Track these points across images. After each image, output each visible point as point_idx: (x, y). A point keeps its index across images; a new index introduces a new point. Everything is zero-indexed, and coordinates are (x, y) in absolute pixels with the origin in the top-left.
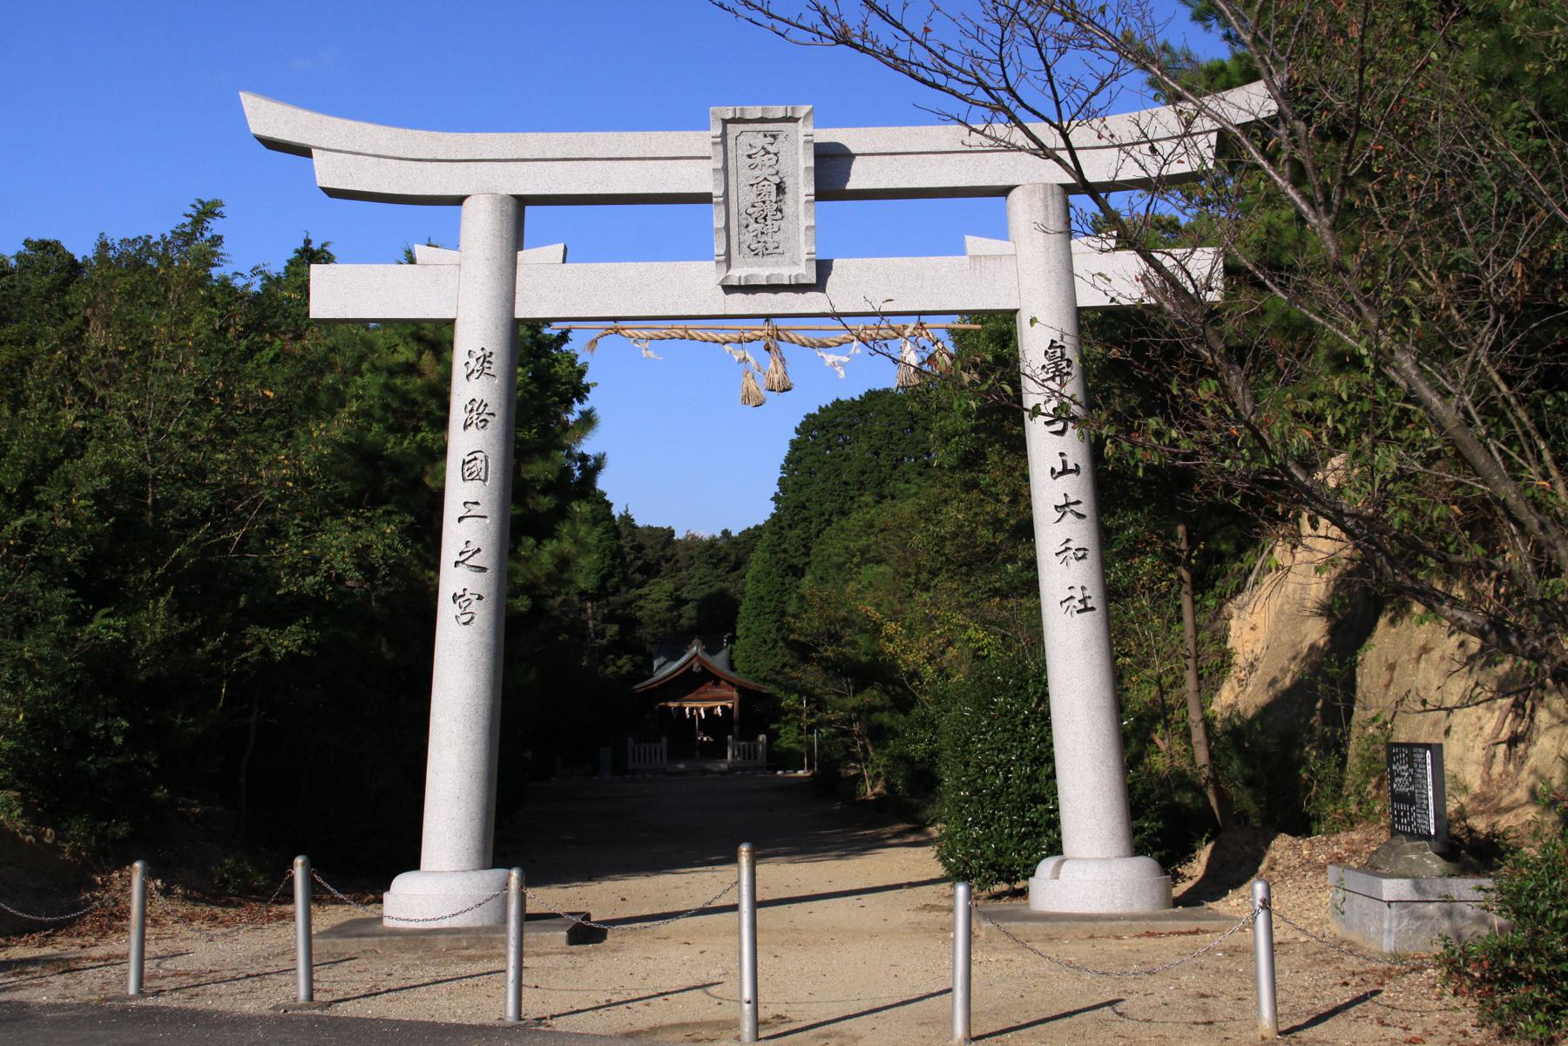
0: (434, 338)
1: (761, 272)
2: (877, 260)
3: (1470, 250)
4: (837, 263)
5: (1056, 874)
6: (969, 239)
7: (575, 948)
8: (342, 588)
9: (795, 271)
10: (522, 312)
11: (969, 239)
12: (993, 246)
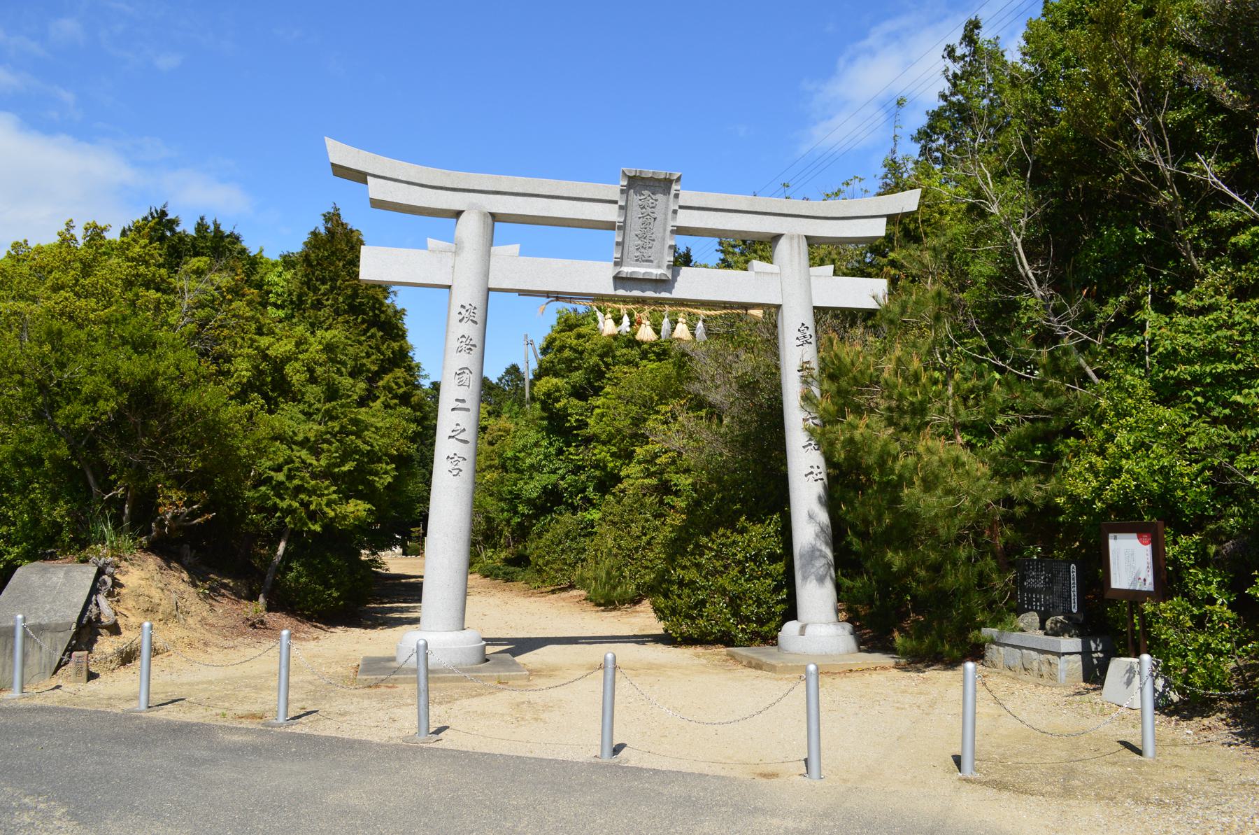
0: (773, 311)
1: (641, 270)
3: (170, 354)
9: (659, 271)
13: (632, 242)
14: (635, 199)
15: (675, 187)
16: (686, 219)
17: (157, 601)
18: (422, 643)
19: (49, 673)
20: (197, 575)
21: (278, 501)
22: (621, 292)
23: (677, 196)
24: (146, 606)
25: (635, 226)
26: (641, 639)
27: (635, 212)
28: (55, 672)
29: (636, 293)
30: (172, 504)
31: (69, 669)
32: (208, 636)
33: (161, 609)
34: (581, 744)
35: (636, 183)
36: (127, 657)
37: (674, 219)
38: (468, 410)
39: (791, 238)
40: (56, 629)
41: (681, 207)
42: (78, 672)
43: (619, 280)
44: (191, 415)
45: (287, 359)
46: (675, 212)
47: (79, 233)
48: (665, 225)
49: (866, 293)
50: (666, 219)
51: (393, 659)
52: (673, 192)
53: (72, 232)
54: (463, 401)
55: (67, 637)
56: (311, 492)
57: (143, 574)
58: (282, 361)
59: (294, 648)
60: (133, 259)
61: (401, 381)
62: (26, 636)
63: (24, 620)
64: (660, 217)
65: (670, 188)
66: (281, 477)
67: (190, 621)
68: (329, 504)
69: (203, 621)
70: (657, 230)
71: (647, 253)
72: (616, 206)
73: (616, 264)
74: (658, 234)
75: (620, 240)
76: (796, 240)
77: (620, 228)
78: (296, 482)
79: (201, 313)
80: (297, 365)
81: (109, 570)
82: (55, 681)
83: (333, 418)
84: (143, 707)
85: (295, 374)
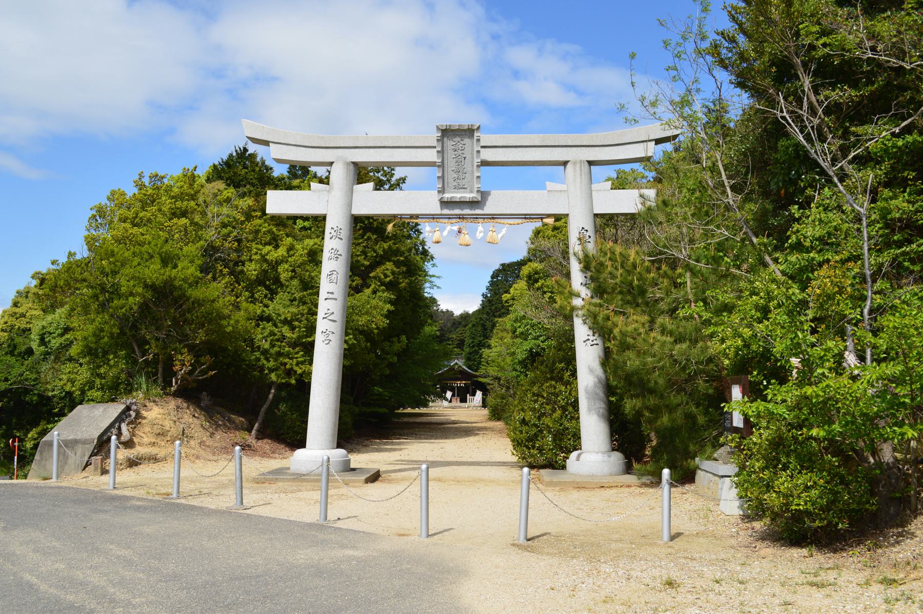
1: (458, 196)
2: (508, 192)
4: (492, 192)
5: (578, 458)
6: (548, 183)
7: (363, 460)
8: (715, 266)
9: (471, 195)
10: (356, 211)
11: (548, 183)
12: (559, 187)
13: (450, 176)
14: (449, 143)
15: (476, 134)
16: (488, 155)
17: (168, 428)
18: (325, 458)
19: (80, 470)
20: (209, 412)
21: (265, 362)
22: (446, 211)
23: (478, 140)
24: (158, 431)
25: (451, 164)
26: (504, 464)
27: (450, 154)
28: (84, 469)
29: (457, 211)
30: (183, 362)
31: (91, 468)
32: (202, 453)
33: (170, 434)
34: (311, 514)
35: (446, 133)
36: (132, 463)
37: (478, 157)
38: (336, 299)
39: (575, 163)
40: (85, 442)
41: (482, 147)
42: (96, 469)
43: (444, 204)
44: (199, 303)
45: (278, 262)
46: (478, 152)
47: (146, 181)
48: (473, 161)
49: (627, 202)
50: (473, 158)
51: (289, 469)
52: (475, 138)
53: (143, 180)
54: (332, 293)
55: (90, 448)
56: (288, 355)
57: (161, 411)
58: (276, 262)
59: (245, 459)
60: (173, 197)
61: (388, 273)
62: (59, 446)
63: (59, 435)
64: (468, 156)
65: (473, 135)
66: (267, 346)
67: (192, 442)
68: (297, 364)
69: (202, 443)
70: (467, 166)
71: (462, 183)
72: (435, 150)
73: (439, 192)
74: (468, 168)
75: (440, 175)
76: (578, 165)
77: (439, 166)
78: (276, 349)
79: (225, 231)
80: (286, 266)
81: (134, 407)
82: (85, 474)
83: (305, 303)
84: (111, 487)
85: (284, 272)
